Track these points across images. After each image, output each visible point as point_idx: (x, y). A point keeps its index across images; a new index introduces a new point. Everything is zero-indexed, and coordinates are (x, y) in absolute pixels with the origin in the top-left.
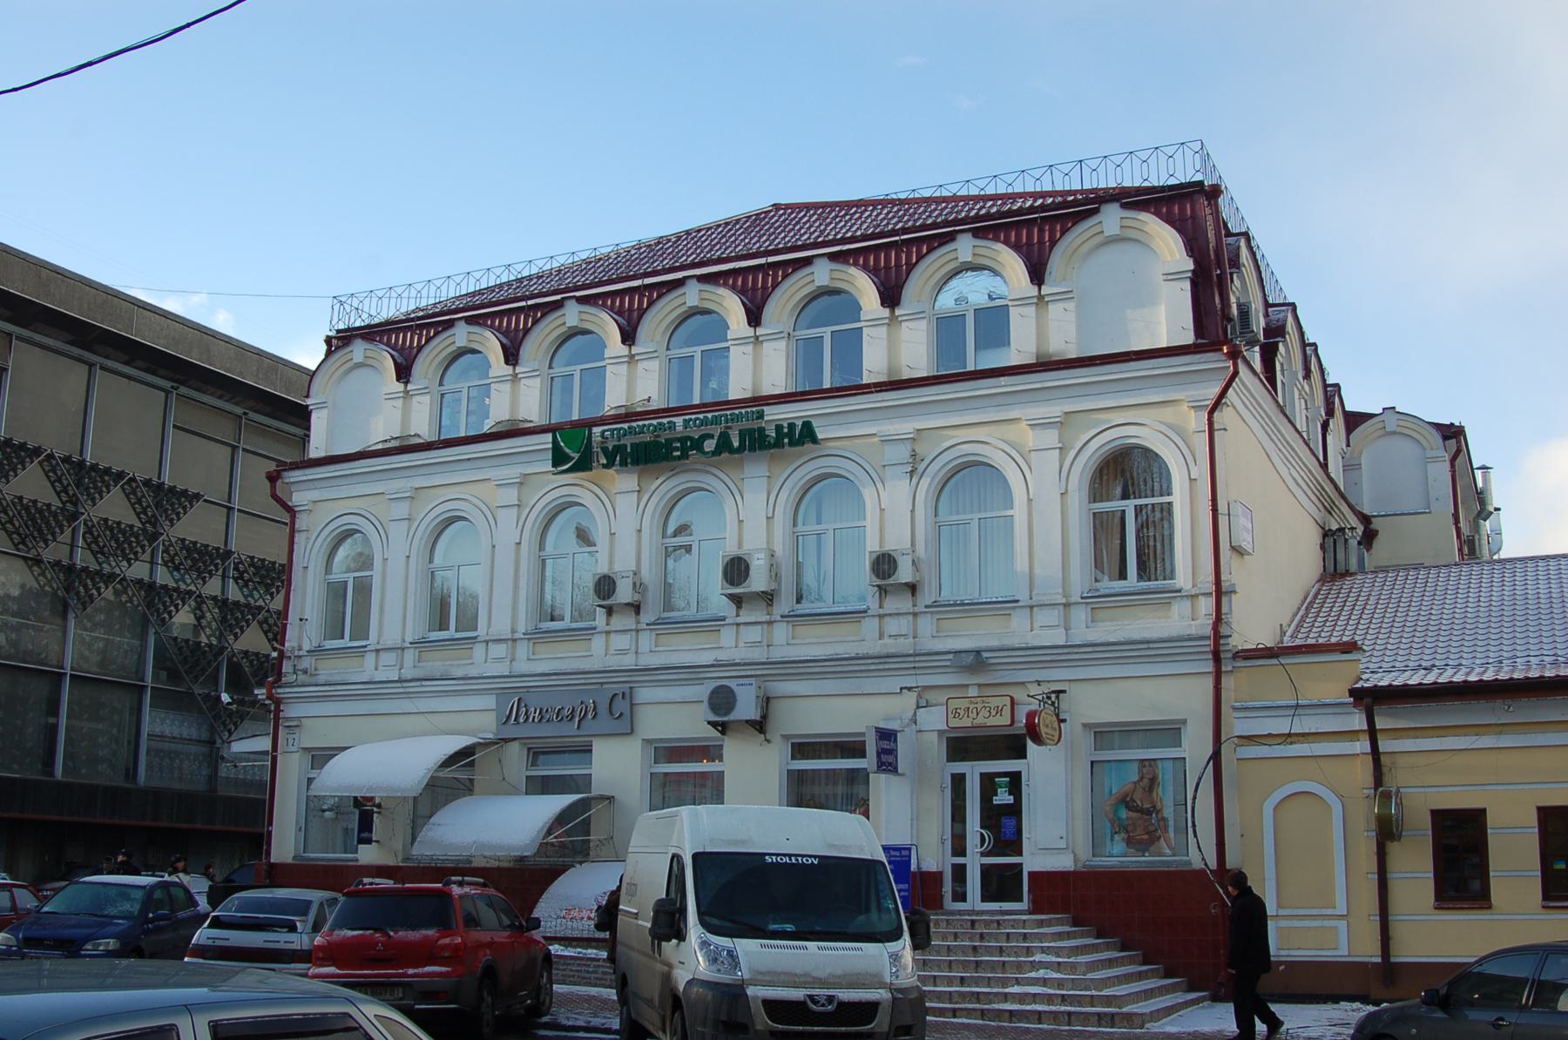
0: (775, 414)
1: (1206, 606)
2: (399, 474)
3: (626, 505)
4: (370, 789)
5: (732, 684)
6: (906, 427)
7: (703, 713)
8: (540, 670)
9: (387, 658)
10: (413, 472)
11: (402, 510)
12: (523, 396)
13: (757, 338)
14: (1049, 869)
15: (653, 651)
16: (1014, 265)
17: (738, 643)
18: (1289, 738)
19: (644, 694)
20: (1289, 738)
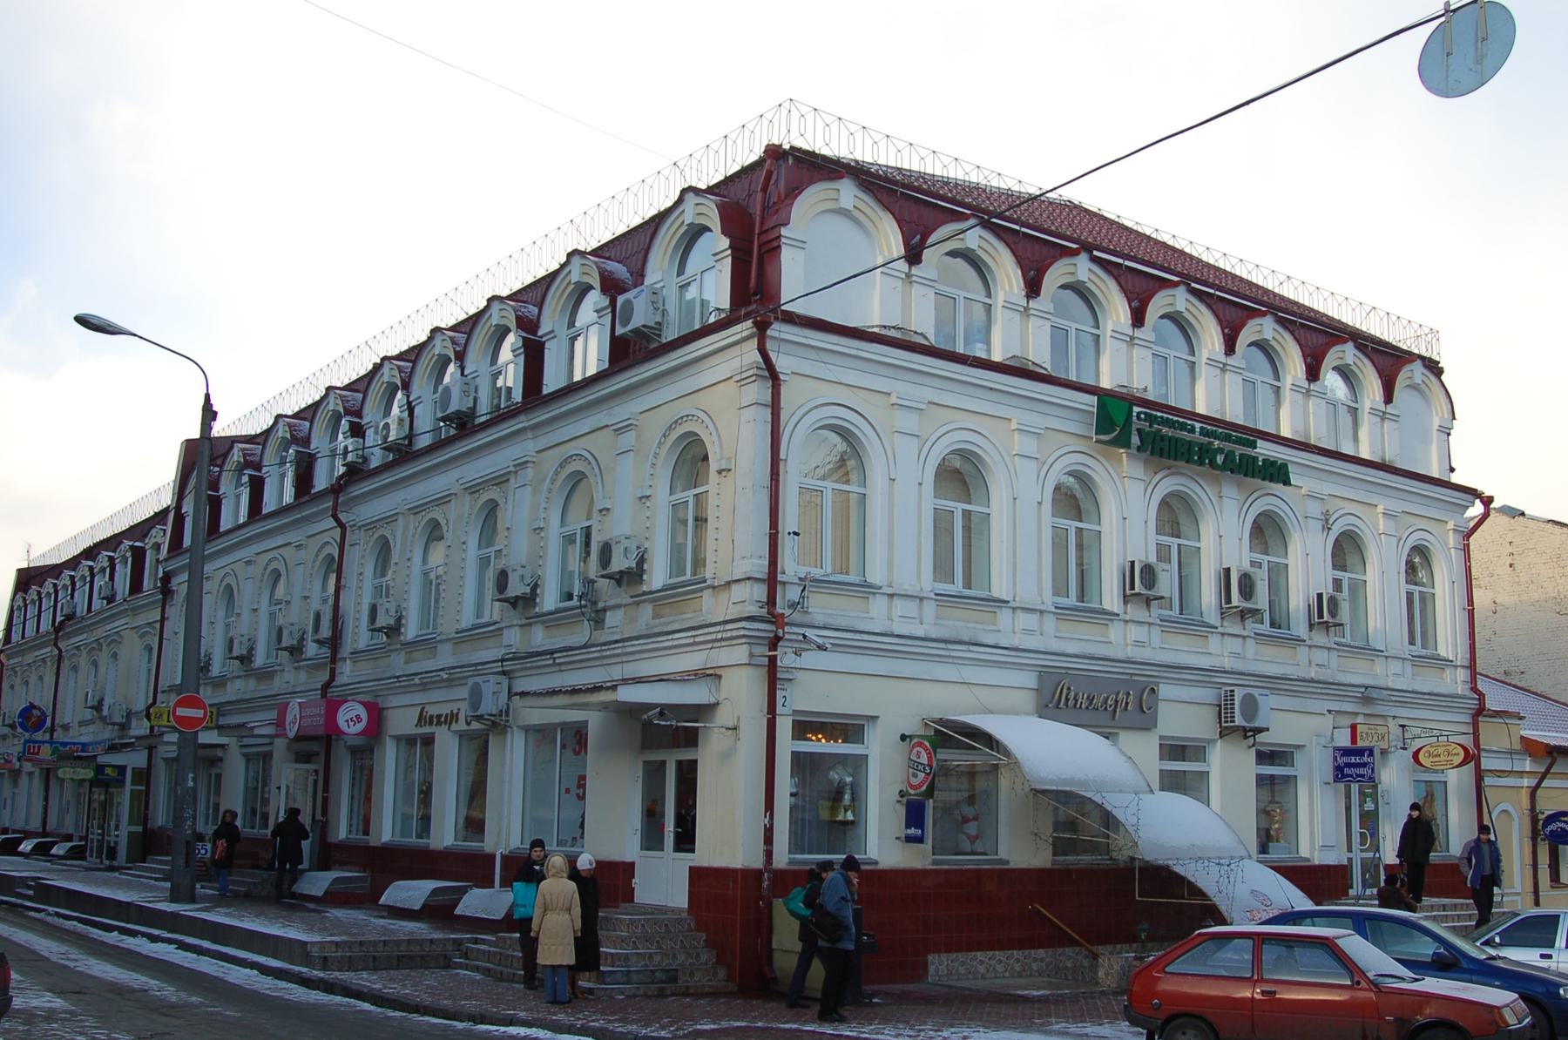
0: (1264, 450)
1: (760, 592)
2: (908, 376)
3: (1135, 490)
4: (1085, 784)
5: (1255, 692)
6: (1326, 488)
7: (1209, 715)
8: (1070, 650)
9: (900, 606)
10: (926, 380)
11: (908, 421)
12: (1017, 332)
13: (1026, 309)
14: (1025, 866)
15: (1182, 650)
16: (892, 240)
17: (1226, 651)
18: (1509, 773)
19: (1165, 690)
20: (1509, 773)
